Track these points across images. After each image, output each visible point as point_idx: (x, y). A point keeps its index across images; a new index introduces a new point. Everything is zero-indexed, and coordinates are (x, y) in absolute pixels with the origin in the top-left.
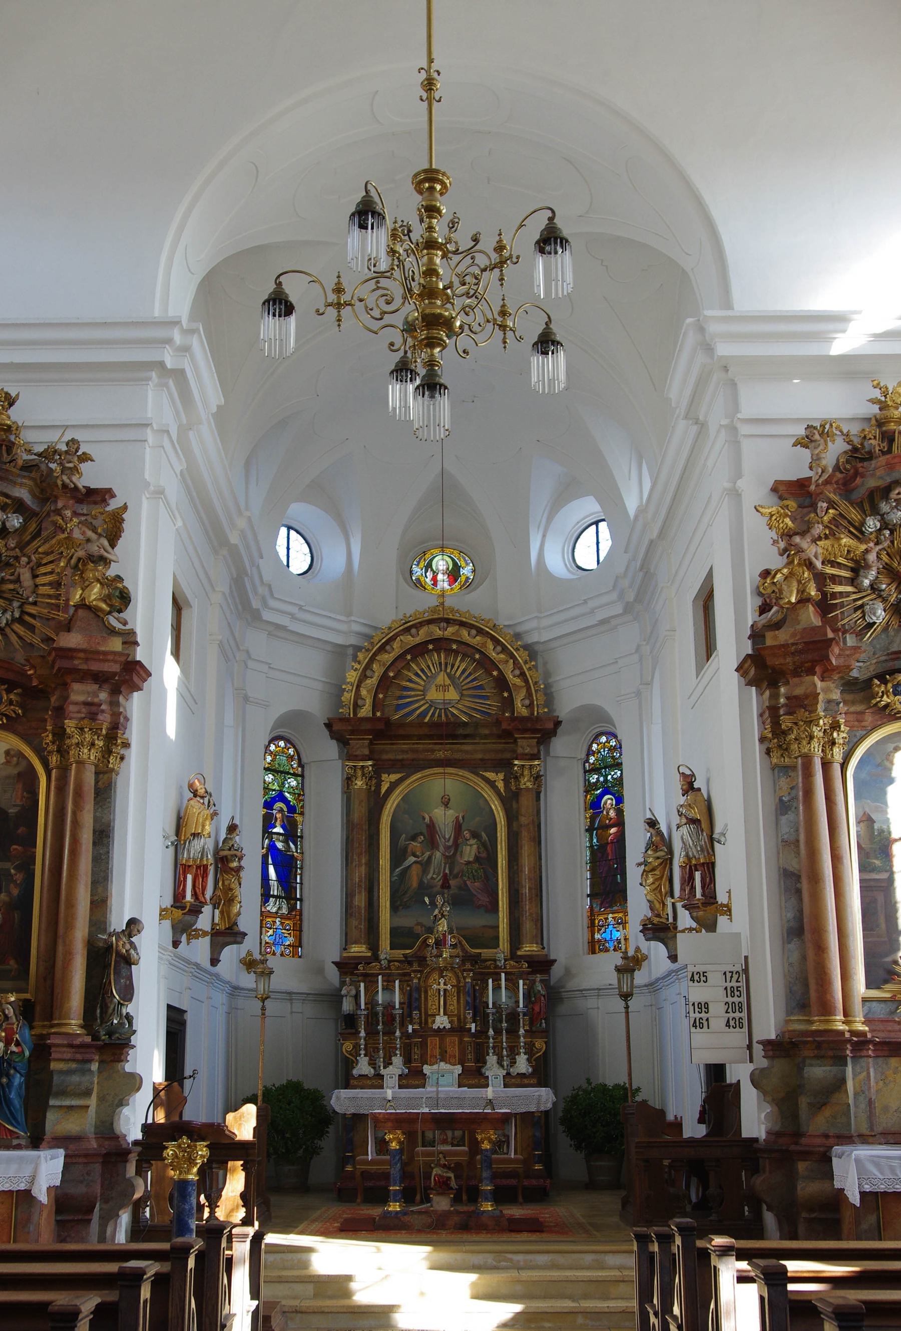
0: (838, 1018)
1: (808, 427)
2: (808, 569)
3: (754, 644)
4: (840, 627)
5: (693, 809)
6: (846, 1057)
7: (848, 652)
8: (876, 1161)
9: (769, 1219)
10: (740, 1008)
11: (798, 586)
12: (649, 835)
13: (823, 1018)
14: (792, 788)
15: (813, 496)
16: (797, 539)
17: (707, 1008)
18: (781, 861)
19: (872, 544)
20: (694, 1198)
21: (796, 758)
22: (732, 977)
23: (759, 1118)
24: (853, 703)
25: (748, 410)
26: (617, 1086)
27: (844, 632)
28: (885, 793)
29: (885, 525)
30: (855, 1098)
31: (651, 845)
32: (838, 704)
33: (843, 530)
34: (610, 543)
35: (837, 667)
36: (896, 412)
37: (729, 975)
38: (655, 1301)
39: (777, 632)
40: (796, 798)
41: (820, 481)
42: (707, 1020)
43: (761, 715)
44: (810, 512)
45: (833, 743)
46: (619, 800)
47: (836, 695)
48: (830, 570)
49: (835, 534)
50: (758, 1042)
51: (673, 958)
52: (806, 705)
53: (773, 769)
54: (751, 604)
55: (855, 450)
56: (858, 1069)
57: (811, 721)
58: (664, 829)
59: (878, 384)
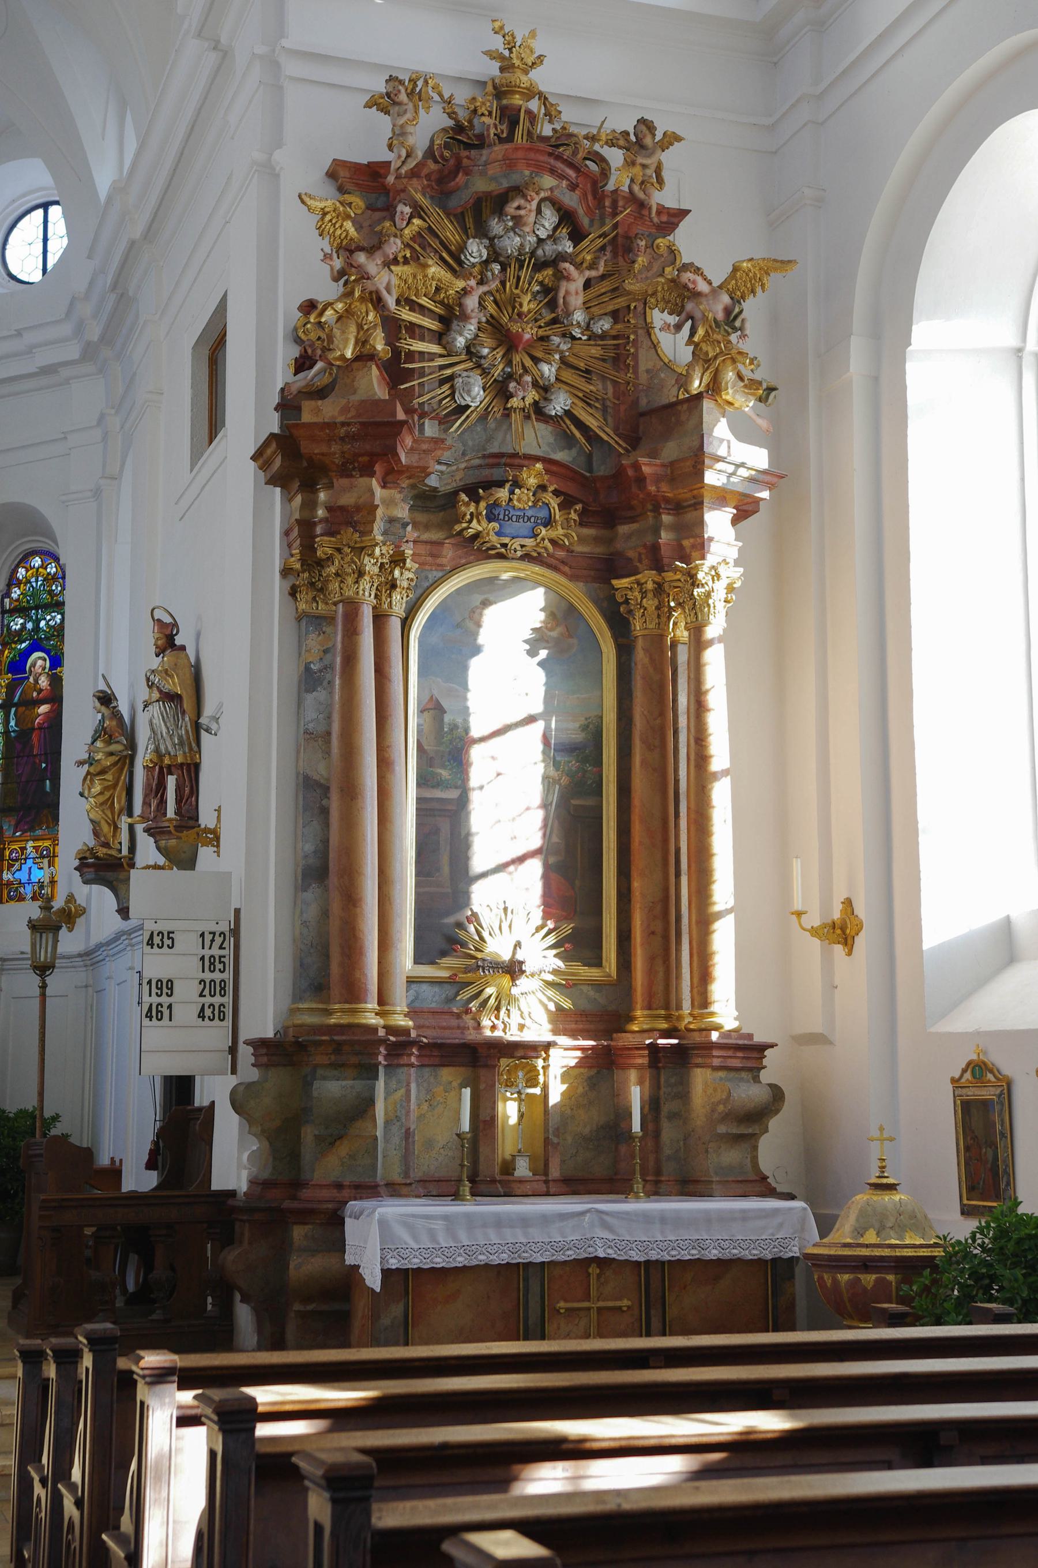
0: (369, 1006)
1: (391, 79)
2: (375, 308)
3: (283, 418)
4: (416, 406)
5: (172, 677)
6: (376, 1066)
7: (425, 446)
8: (407, 1222)
9: (244, 1315)
10: (223, 989)
11: (358, 333)
12: (99, 716)
13: (347, 1006)
14: (325, 651)
15: (391, 194)
16: (361, 258)
17: (171, 989)
18: (301, 763)
19: (473, 282)
20: (131, 1287)
21: (335, 604)
22: (213, 941)
23: (239, 1159)
24: (427, 527)
25: (296, 37)
26: (22, 1113)
27: (423, 415)
28: (465, 668)
29: (495, 255)
30: (385, 1127)
31: (101, 733)
32: (405, 525)
33: (432, 254)
34: (65, 242)
35: (408, 468)
36: (524, 78)
37: (208, 938)
38: (44, 1460)
39: (320, 402)
40: (329, 667)
41: (403, 171)
42: (170, 1007)
43: (287, 533)
44: (384, 219)
45: (393, 586)
46: (56, 661)
47: (403, 512)
48: (407, 315)
49: (418, 258)
50: (247, 1043)
51: (124, 912)
52: (355, 522)
53: (299, 619)
54: (284, 354)
55: (459, 128)
56: (393, 1085)
57: (363, 548)
58: (124, 709)
59: (502, 28)
